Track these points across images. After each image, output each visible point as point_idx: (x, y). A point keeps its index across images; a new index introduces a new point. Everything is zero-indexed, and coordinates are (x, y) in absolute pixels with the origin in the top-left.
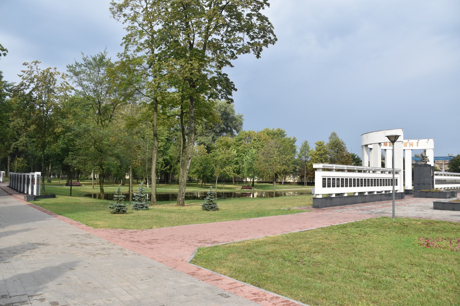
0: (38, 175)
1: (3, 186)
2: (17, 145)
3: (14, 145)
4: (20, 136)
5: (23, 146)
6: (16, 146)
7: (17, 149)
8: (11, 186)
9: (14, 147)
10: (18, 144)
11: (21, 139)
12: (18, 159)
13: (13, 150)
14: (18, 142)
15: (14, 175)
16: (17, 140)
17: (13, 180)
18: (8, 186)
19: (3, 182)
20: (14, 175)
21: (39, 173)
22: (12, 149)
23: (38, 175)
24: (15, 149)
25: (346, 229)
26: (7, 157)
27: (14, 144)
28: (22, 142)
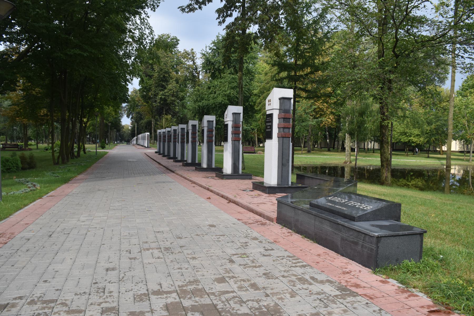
0: (148, 135)
1: (150, 153)
2: (165, 95)
3: (161, 95)
4: (168, 83)
5: (173, 96)
6: (163, 97)
7: (165, 100)
8: (162, 152)
9: (161, 98)
10: (167, 94)
11: (170, 87)
12: (166, 116)
13: (160, 103)
14: (166, 91)
15: (162, 133)
16: (165, 88)
17: (164, 141)
18: (156, 152)
19: (148, 147)
20: (162, 133)
21: (149, 133)
22: (159, 101)
23: (148, 135)
24: (162, 100)
25: (371, 72)
26: (151, 121)
27: (161, 93)
28: (171, 90)
